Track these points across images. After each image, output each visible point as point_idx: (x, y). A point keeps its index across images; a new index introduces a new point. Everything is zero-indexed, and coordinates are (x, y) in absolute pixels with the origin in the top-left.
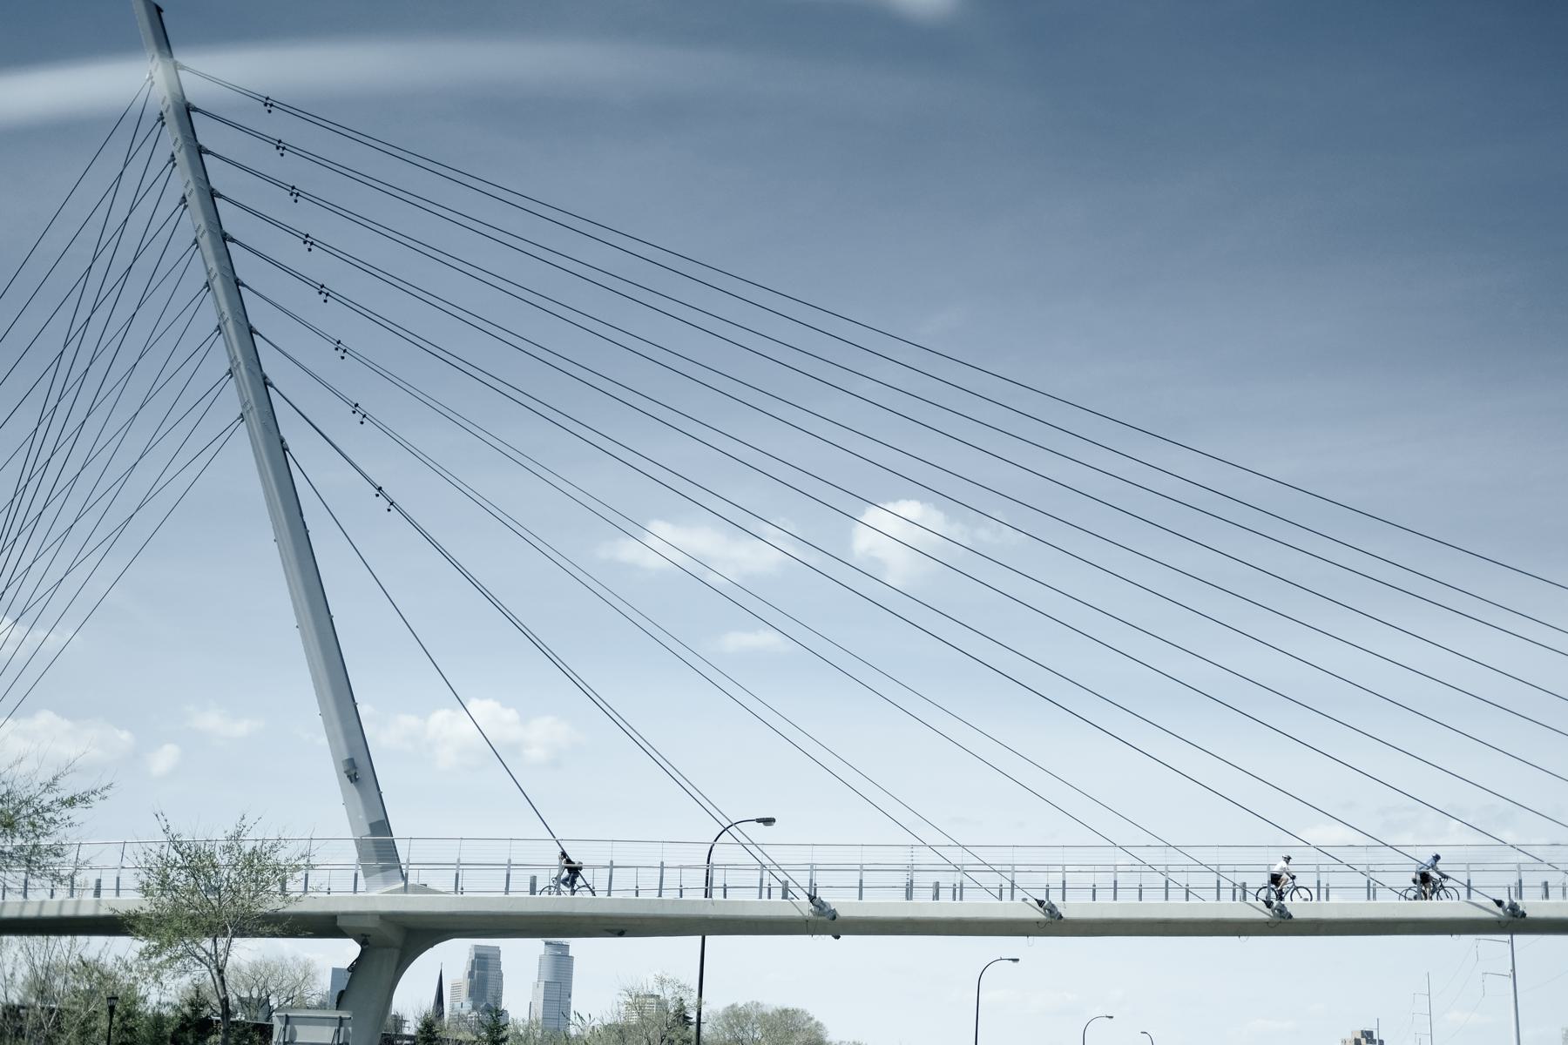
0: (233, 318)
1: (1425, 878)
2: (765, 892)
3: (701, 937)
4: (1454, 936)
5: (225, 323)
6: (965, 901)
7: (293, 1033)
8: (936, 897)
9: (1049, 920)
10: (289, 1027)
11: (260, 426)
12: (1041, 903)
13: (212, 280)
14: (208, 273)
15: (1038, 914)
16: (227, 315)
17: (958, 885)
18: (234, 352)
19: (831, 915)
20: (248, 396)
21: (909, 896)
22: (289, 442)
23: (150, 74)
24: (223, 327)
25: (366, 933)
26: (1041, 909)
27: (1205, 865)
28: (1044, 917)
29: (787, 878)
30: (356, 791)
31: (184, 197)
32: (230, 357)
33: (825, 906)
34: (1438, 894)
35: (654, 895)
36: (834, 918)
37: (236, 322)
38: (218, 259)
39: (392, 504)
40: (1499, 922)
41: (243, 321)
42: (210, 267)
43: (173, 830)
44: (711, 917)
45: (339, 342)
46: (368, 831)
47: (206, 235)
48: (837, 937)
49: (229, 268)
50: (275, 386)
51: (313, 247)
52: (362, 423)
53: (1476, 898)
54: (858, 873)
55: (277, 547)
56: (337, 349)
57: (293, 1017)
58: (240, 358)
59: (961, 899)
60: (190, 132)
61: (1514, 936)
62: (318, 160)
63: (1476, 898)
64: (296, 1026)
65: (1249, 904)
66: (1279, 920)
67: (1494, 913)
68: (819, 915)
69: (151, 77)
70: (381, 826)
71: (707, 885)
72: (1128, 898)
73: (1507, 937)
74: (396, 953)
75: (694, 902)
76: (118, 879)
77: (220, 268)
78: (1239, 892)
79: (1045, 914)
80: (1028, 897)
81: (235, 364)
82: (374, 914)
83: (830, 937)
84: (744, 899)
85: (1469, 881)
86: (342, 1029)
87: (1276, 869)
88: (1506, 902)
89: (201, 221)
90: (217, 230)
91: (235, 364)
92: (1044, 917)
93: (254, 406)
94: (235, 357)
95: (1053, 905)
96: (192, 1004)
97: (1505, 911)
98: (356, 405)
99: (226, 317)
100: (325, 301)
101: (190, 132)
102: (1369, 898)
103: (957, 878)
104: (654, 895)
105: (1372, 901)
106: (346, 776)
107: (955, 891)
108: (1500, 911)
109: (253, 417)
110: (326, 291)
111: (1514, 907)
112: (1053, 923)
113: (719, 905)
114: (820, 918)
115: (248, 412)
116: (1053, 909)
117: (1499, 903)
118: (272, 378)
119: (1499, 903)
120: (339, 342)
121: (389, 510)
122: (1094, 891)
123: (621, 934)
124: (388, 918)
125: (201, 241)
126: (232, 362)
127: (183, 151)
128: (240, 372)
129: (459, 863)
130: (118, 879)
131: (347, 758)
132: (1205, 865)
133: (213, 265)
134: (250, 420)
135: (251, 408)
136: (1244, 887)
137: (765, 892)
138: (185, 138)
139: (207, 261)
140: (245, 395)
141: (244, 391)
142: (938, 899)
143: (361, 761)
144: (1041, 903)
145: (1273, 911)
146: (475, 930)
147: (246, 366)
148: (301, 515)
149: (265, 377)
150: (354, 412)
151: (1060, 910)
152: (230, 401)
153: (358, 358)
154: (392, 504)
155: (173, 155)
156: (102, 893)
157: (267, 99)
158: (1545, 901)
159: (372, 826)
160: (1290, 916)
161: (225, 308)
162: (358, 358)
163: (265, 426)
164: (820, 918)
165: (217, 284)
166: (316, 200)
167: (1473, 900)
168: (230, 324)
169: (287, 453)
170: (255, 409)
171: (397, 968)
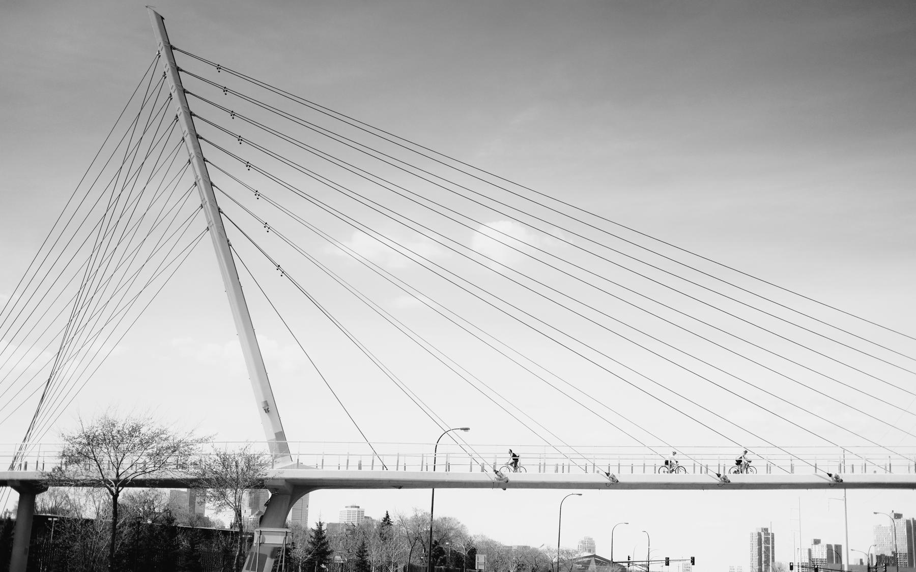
0: (203, 178)
1: (739, 462)
2: (425, 467)
3: (432, 489)
4: (809, 490)
5: (198, 181)
6: (546, 473)
7: (264, 539)
8: (557, 471)
9: (612, 482)
10: (261, 536)
11: (217, 233)
12: (608, 474)
13: (192, 159)
14: (190, 156)
15: (607, 480)
16: (200, 177)
17: (864, 465)
18: (204, 196)
19: (506, 480)
20: (211, 219)
21: (360, 468)
22: (231, 242)
23: (159, 52)
24: (197, 183)
25: (276, 488)
26: (608, 477)
27: (686, 455)
28: (609, 481)
29: (484, 462)
30: (268, 417)
31: (177, 116)
32: (201, 198)
33: (503, 475)
34: (747, 470)
35: (369, 469)
36: (507, 481)
37: (205, 181)
38: (195, 148)
39: (283, 272)
40: (830, 484)
41: (208, 180)
42: (190, 153)
43: (66, 435)
44: (446, 481)
45: (257, 191)
46: (274, 437)
47: (189, 136)
48: (505, 489)
49: (200, 153)
50: (224, 212)
51: (242, 142)
52: (268, 232)
53: (819, 472)
54: (346, 456)
55: (226, 295)
56: (256, 195)
57: (264, 531)
58: (207, 199)
59: (544, 471)
60: (179, 82)
61: (846, 490)
62: (240, 95)
63: (819, 472)
64: (265, 536)
65: (710, 475)
66: (835, 482)
67: (828, 480)
68: (500, 480)
69: (159, 53)
70: (280, 435)
71: (449, 466)
72: (638, 471)
73: (843, 490)
74: (289, 497)
75: (440, 473)
76: (323, 460)
77: (196, 153)
78: (704, 469)
79: (610, 480)
80: (600, 470)
81: (204, 202)
82: (282, 479)
83: (501, 489)
84: (460, 472)
85: (816, 464)
86: (287, 537)
87: (668, 459)
88: (722, 475)
89: (185, 128)
90: (194, 133)
91: (204, 202)
92: (609, 481)
93: (214, 223)
94: (204, 199)
95: (614, 476)
96: (168, 520)
97: (833, 479)
98: (266, 223)
99: (199, 178)
100: (249, 170)
101: (179, 82)
102: (767, 472)
103: (566, 462)
104: (369, 469)
105: (769, 474)
106: (263, 409)
107: (446, 466)
108: (830, 478)
109: (214, 229)
110: (249, 165)
111: (837, 477)
112: (614, 484)
113: (440, 474)
114: (501, 481)
115: (211, 227)
116: (614, 478)
117: (830, 475)
118: (222, 209)
119: (830, 475)
120: (257, 191)
121: (282, 276)
122: (632, 467)
123: (400, 488)
124: (289, 481)
125: (185, 138)
126: (202, 201)
127: (176, 92)
128: (207, 207)
129: (349, 455)
130: (323, 460)
131: (263, 400)
132: (686, 455)
133: (192, 151)
134: (212, 230)
135: (213, 224)
136: (707, 467)
137: (425, 467)
138: (177, 85)
139: (189, 149)
140: (209, 218)
141: (208, 214)
142: (361, 469)
143: (270, 402)
144: (608, 474)
145: (721, 479)
146: (332, 486)
147: (210, 203)
148: (238, 279)
149: (219, 209)
150: (265, 227)
151: (618, 478)
152: (202, 220)
153: (265, 198)
154: (283, 272)
155: (171, 94)
156: (362, 467)
157: (219, 65)
158: (852, 474)
159: (276, 434)
160: (729, 482)
161: (199, 173)
162: (265, 198)
163: (220, 233)
164: (501, 481)
165: (195, 161)
166: (241, 117)
167: (817, 474)
168: (201, 181)
169: (230, 247)
170: (215, 225)
171: (290, 504)
